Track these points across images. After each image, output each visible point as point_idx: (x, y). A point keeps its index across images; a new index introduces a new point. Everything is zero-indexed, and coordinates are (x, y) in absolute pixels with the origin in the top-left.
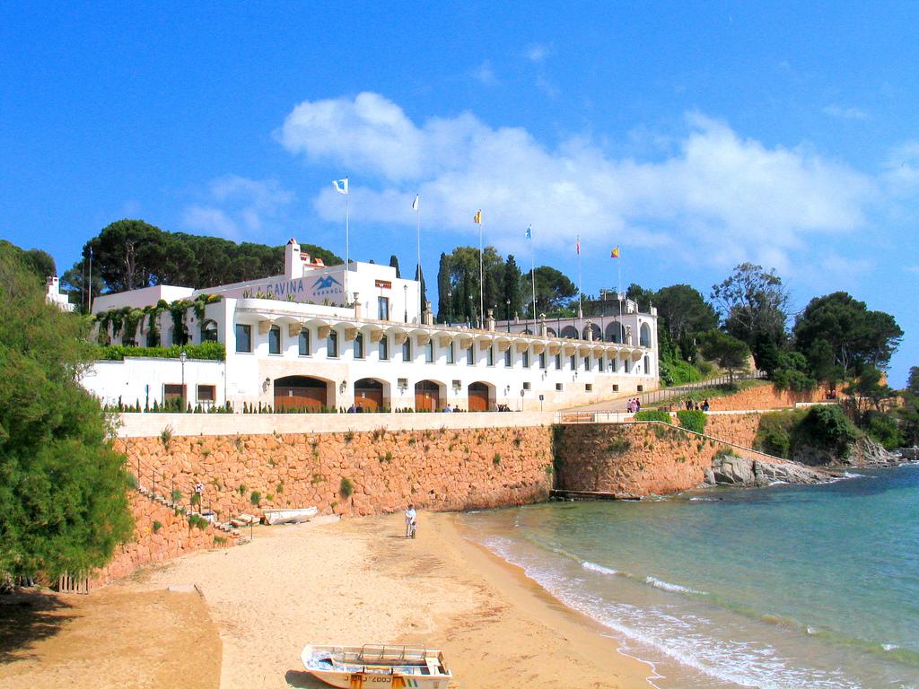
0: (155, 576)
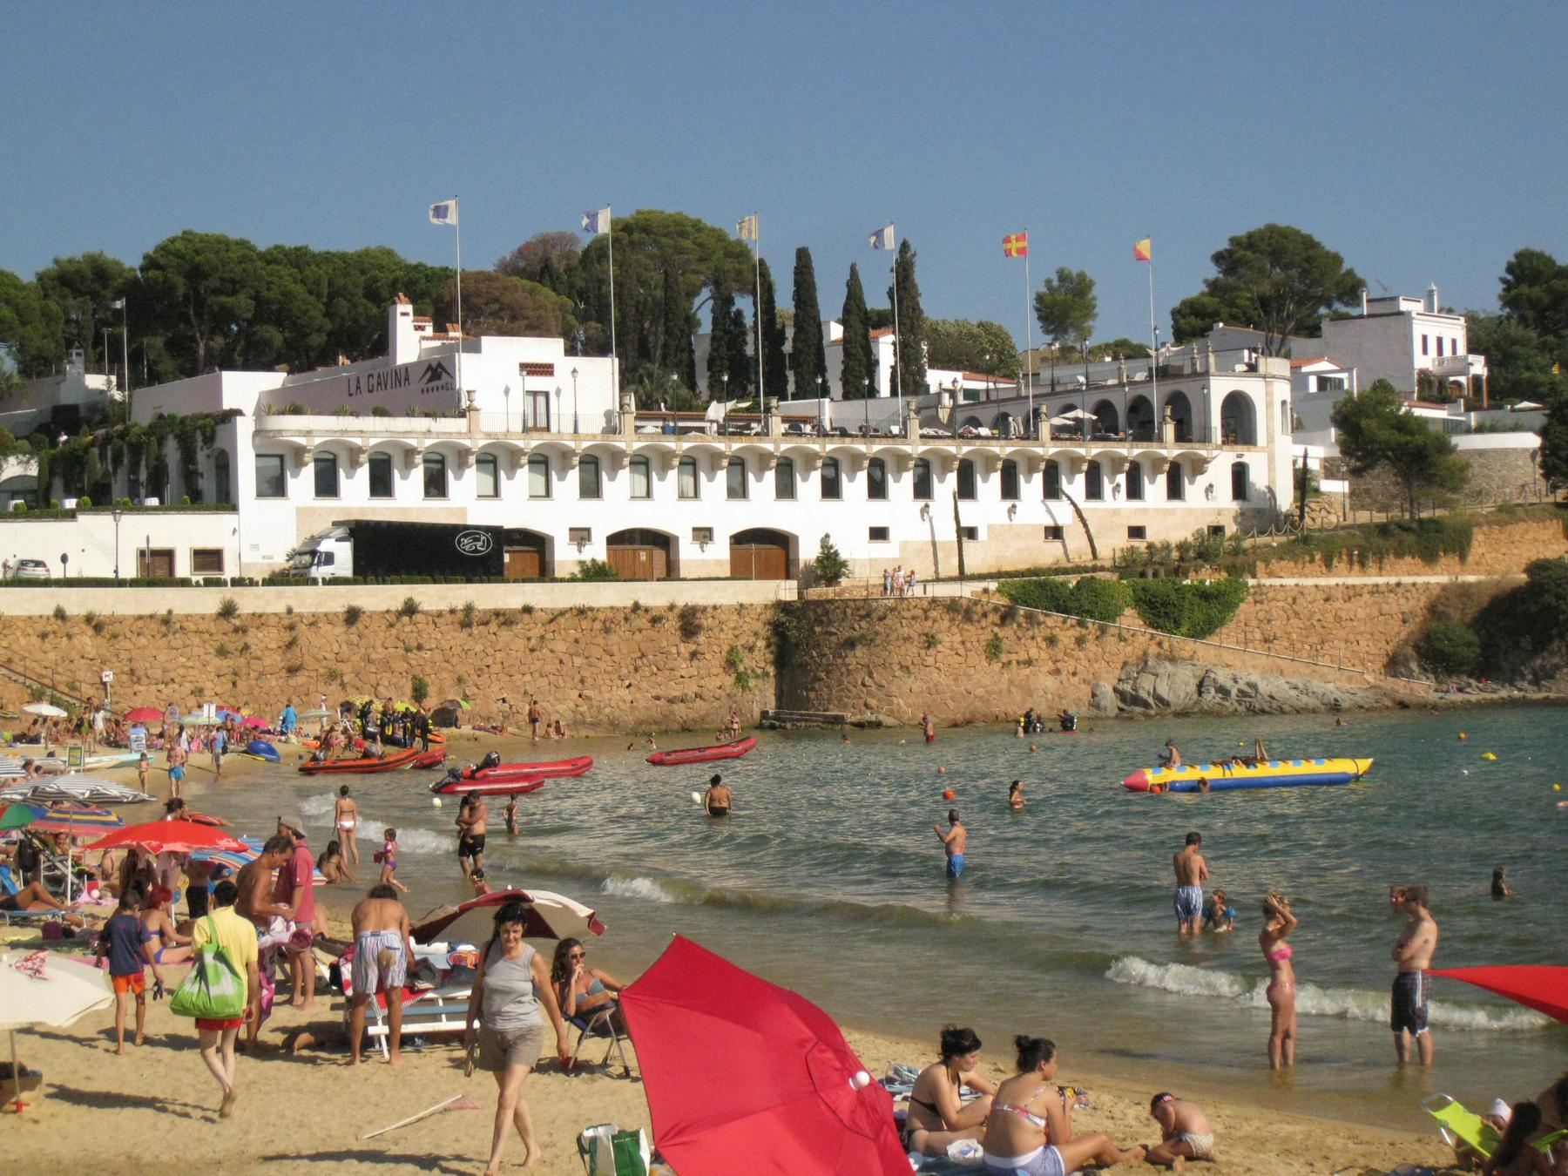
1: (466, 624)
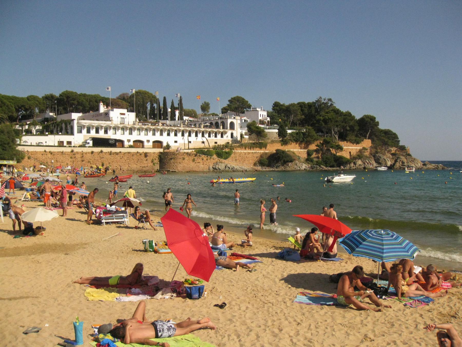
0: (290, 164)
1: (110, 154)
